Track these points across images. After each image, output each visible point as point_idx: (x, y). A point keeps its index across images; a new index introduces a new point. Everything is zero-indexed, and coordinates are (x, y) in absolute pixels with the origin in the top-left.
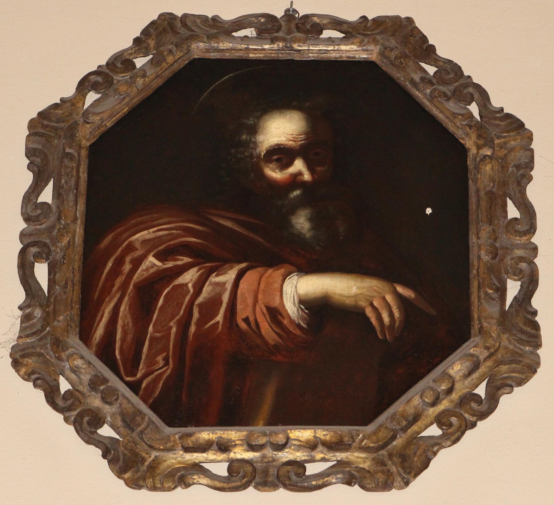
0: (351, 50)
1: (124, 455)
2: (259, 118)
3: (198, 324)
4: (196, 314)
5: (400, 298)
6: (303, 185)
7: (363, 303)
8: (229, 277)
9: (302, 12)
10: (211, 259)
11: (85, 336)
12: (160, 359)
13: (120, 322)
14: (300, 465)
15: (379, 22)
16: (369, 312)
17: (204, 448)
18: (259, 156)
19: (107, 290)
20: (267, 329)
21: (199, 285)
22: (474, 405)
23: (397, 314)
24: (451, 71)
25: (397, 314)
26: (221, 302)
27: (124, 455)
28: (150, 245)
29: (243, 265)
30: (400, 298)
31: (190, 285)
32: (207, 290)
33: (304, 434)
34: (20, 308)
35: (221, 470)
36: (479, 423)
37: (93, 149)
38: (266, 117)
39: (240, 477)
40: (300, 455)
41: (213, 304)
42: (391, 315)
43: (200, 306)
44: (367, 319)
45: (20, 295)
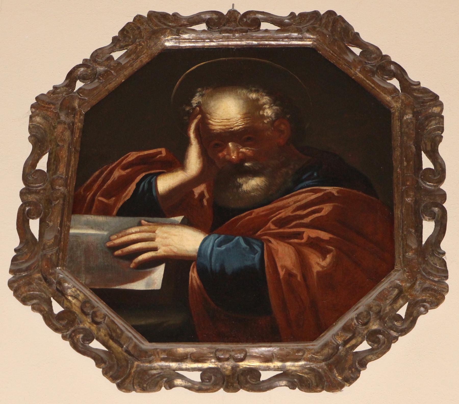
0: (294, 40)
9: (242, 11)
15: (303, 15)
17: (182, 358)
24: (370, 51)
33: (264, 350)
34: (16, 250)
35: (196, 377)
36: (400, 338)
38: (241, 102)
39: (213, 381)
40: (255, 364)
45: (15, 241)
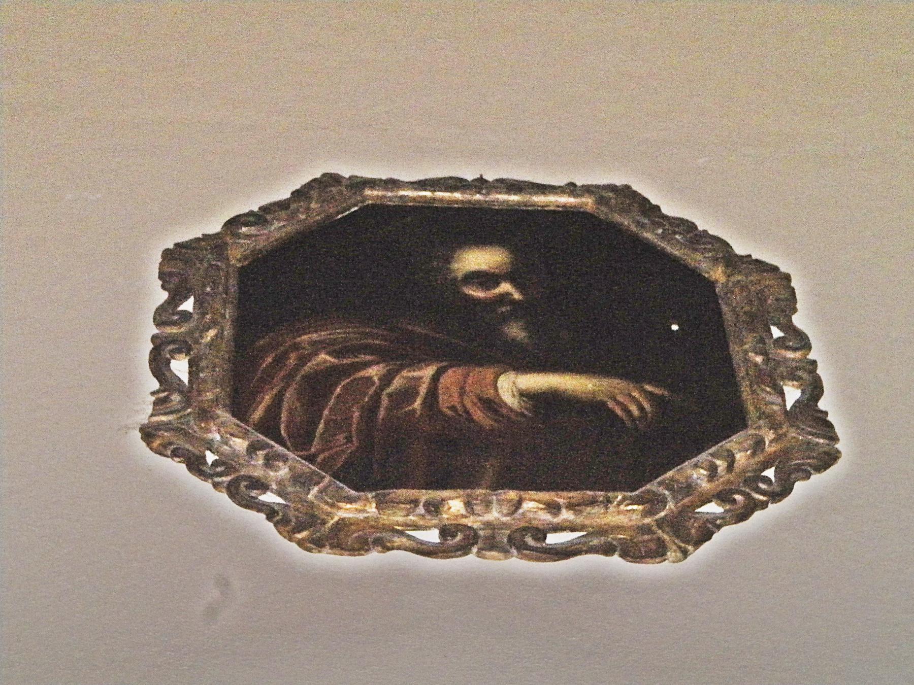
1: (297, 518)
2: (453, 250)
3: (389, 409)
4: (385, 401)
5: (650, 396)
6: (513, 302)
7: (601, 397)
8: (428, 372)
10: (400, 354)
11: (240, 410)
12: (341, 438)
13: (285, 405)
14: (540, 533)
16: (611, 404)
18: (455, 279)
19: (267, 379)
20: (478, 415)
21: (387, 379)
22: (763, 486)
23: (647, 406)
25: (647, 406)
26: (417, 393)
27: (297, 518)
28: (318, 347)
29: (444, 364)
30: (650, 396)
31: (376, 379)
32: (397, 383)
37: (243, 273)
41: (408, 393)
42: (641, 408)
43: (390, 395)
44: (612, 412)
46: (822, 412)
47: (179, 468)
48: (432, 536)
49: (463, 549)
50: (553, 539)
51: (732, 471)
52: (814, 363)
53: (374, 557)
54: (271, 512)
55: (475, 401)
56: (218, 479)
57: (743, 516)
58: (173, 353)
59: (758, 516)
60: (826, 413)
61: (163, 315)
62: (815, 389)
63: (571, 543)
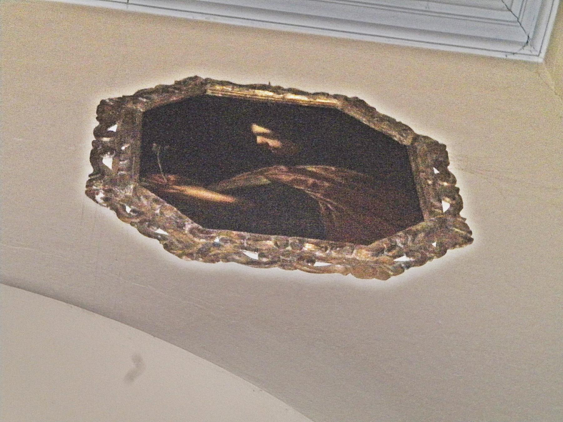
46: (462, 218)
47: (113, 214)
48: (254, 256)
49: (271, 263)
50: (318, 264)
51: (377, 255)
52: (458, 190)
53: (220, 265)
54: (162, 238)
55: (143, 210)
56: (134, 220)
57: (421, 262)
58: (104, 152)
59: (428, 264)
60: (465, 219)
61: (98, 133)
62: (458, 206)
63: (325, 267)
